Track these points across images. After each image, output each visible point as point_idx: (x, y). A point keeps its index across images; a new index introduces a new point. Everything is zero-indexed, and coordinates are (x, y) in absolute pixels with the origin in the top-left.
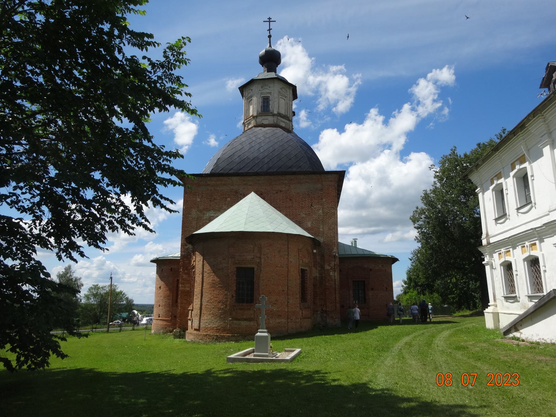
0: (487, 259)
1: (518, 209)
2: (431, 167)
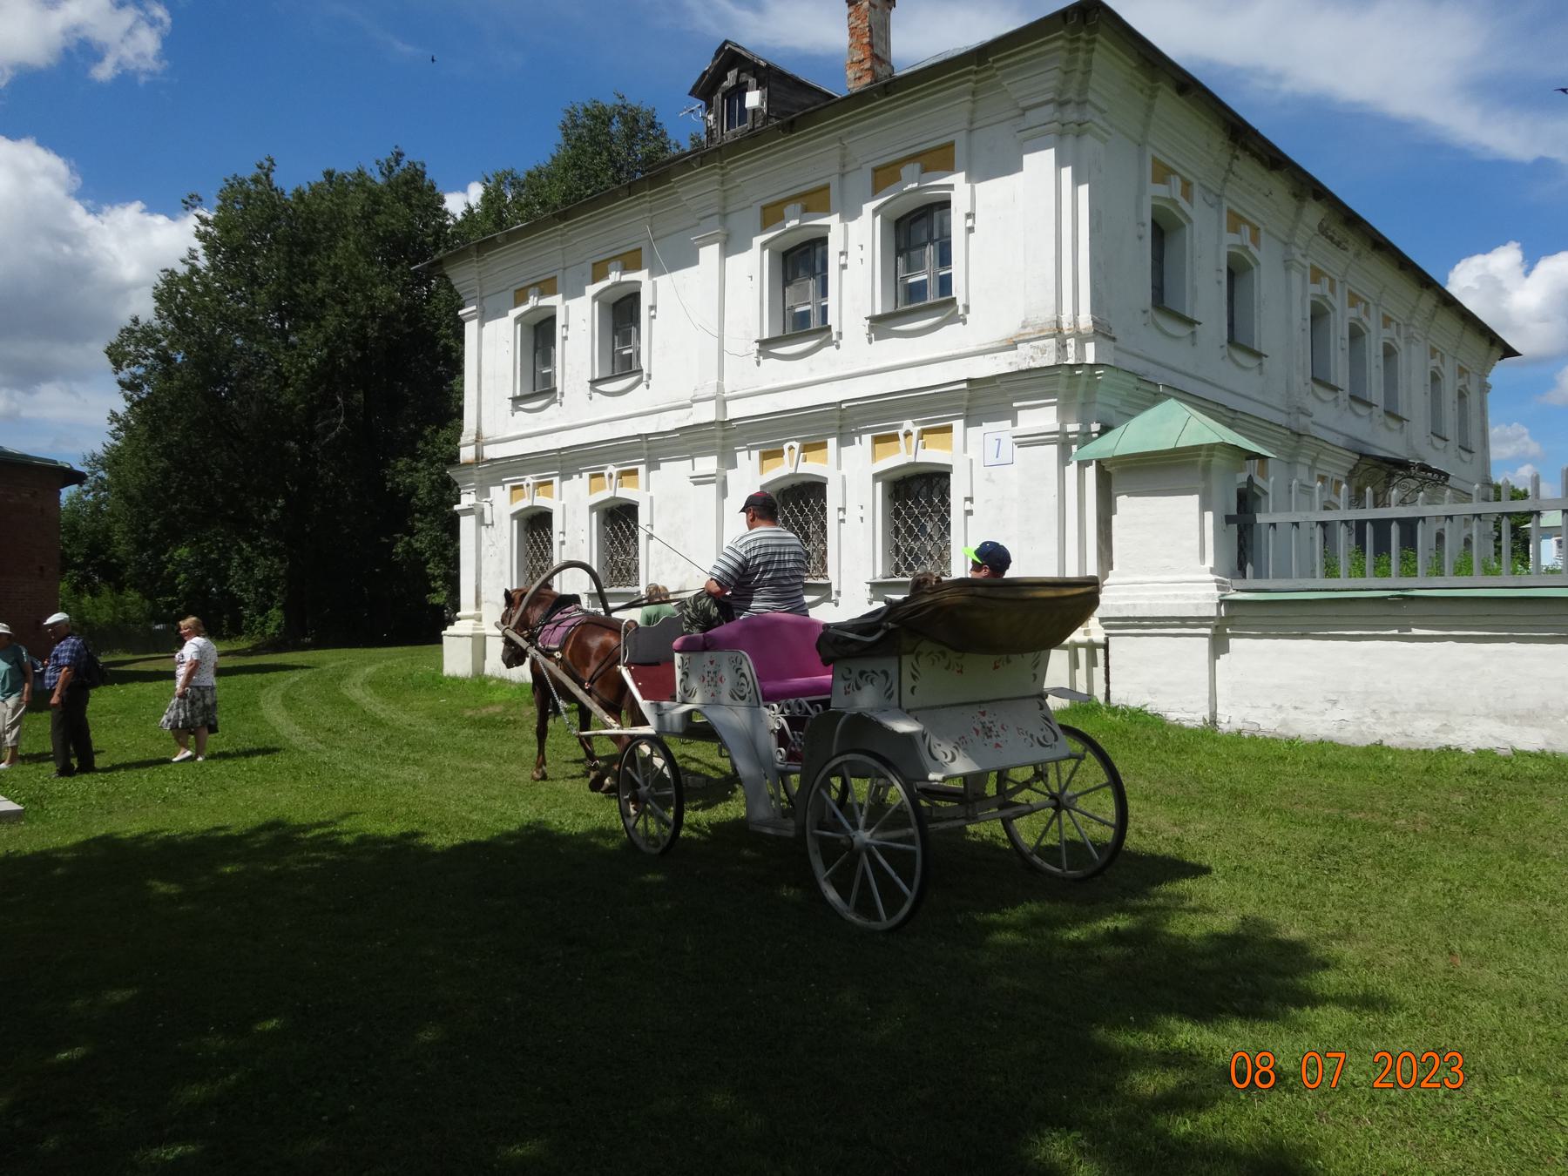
0: (467, 500)
1: (594, 382)
2: (188, 200)
